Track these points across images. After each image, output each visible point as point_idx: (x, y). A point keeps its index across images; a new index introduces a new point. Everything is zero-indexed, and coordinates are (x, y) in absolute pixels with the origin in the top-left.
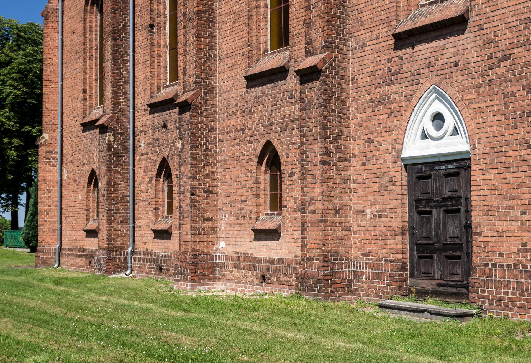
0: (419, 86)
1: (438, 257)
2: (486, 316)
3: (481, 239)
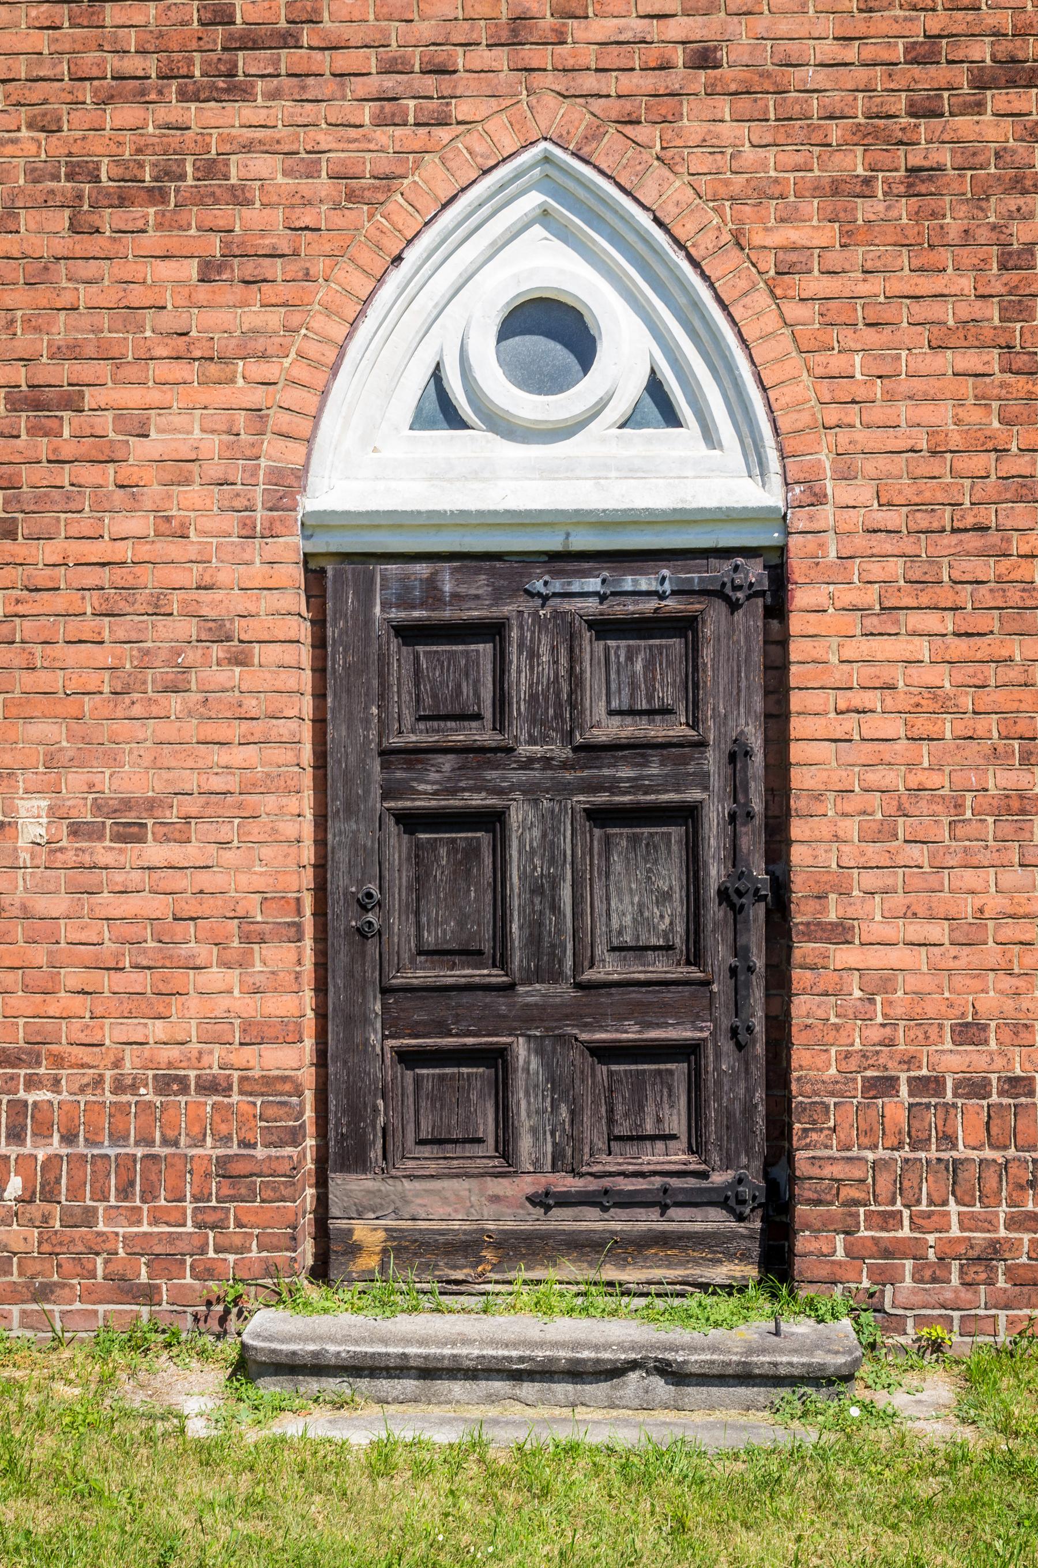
0: (444, 134)
1: (540, 1052)
2: (902, 1340)
3: (844, 956)
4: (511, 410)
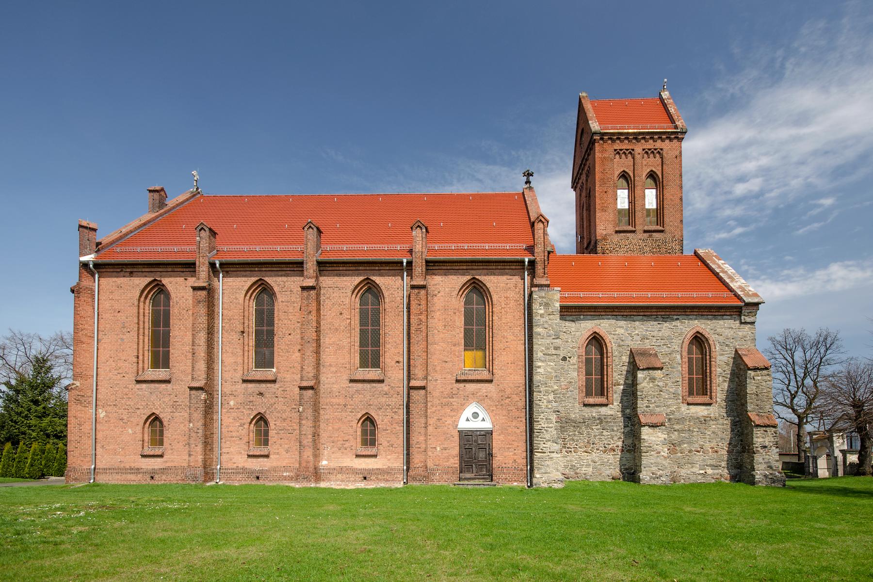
4: (336, 278)
